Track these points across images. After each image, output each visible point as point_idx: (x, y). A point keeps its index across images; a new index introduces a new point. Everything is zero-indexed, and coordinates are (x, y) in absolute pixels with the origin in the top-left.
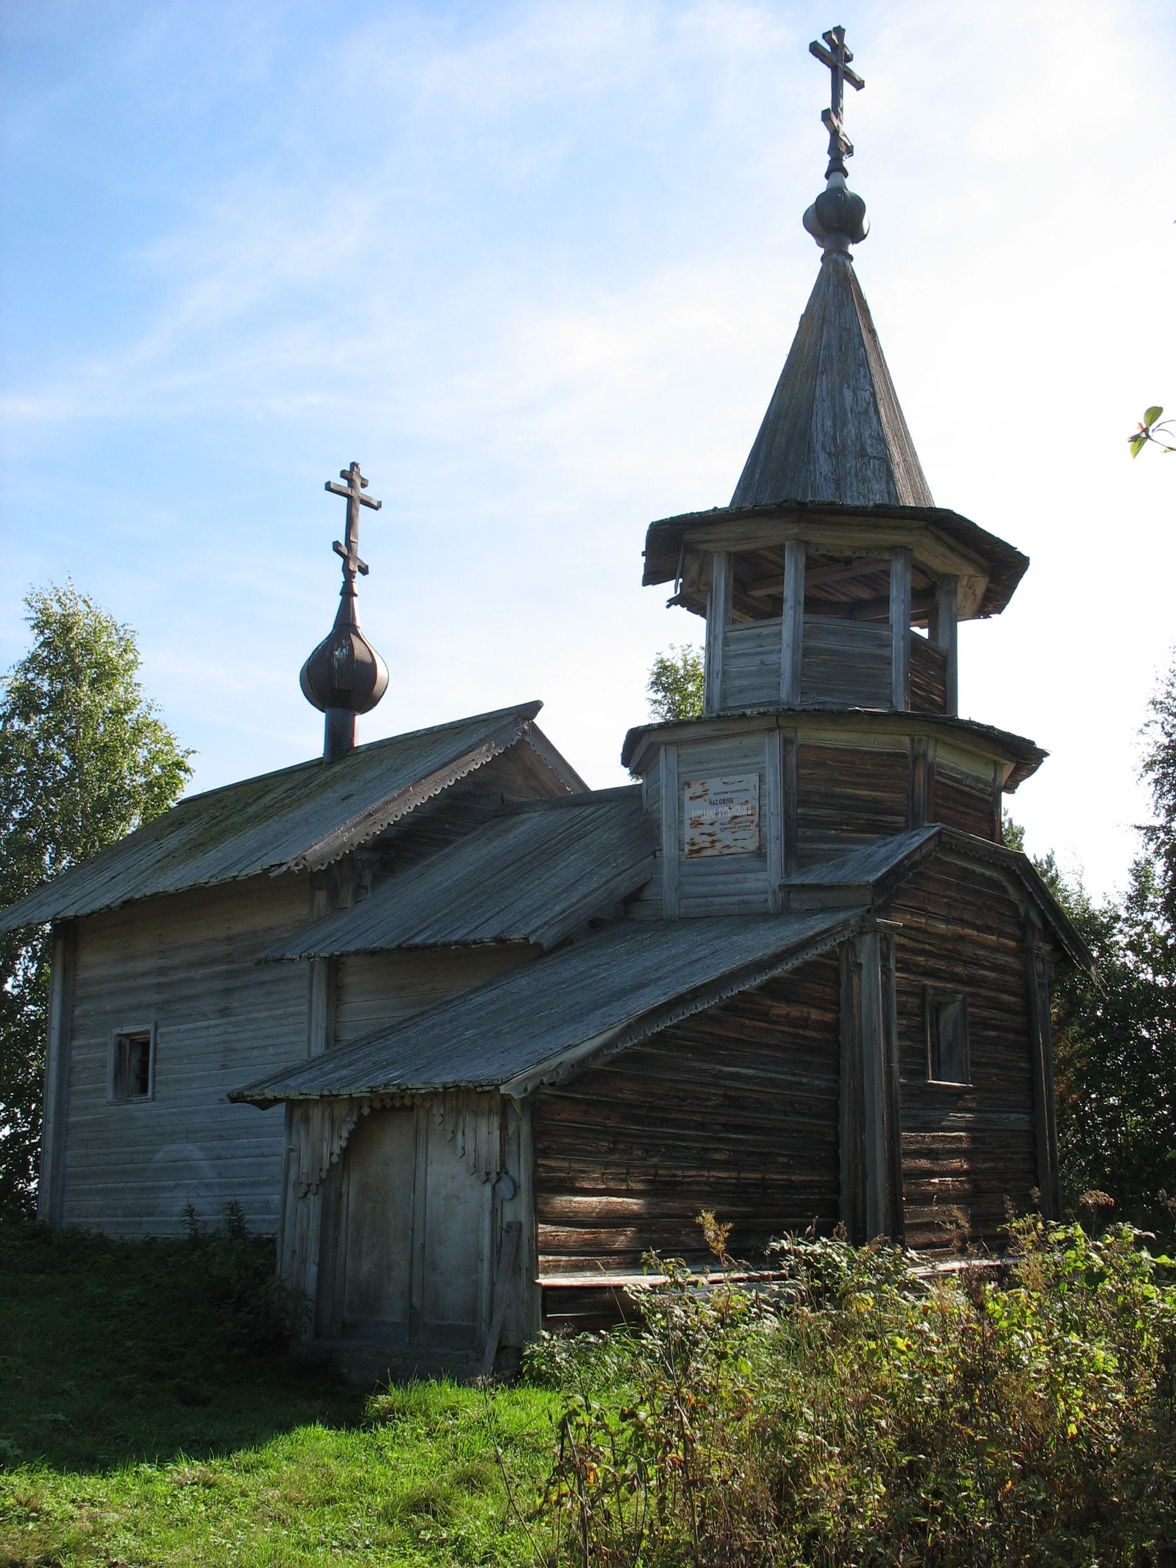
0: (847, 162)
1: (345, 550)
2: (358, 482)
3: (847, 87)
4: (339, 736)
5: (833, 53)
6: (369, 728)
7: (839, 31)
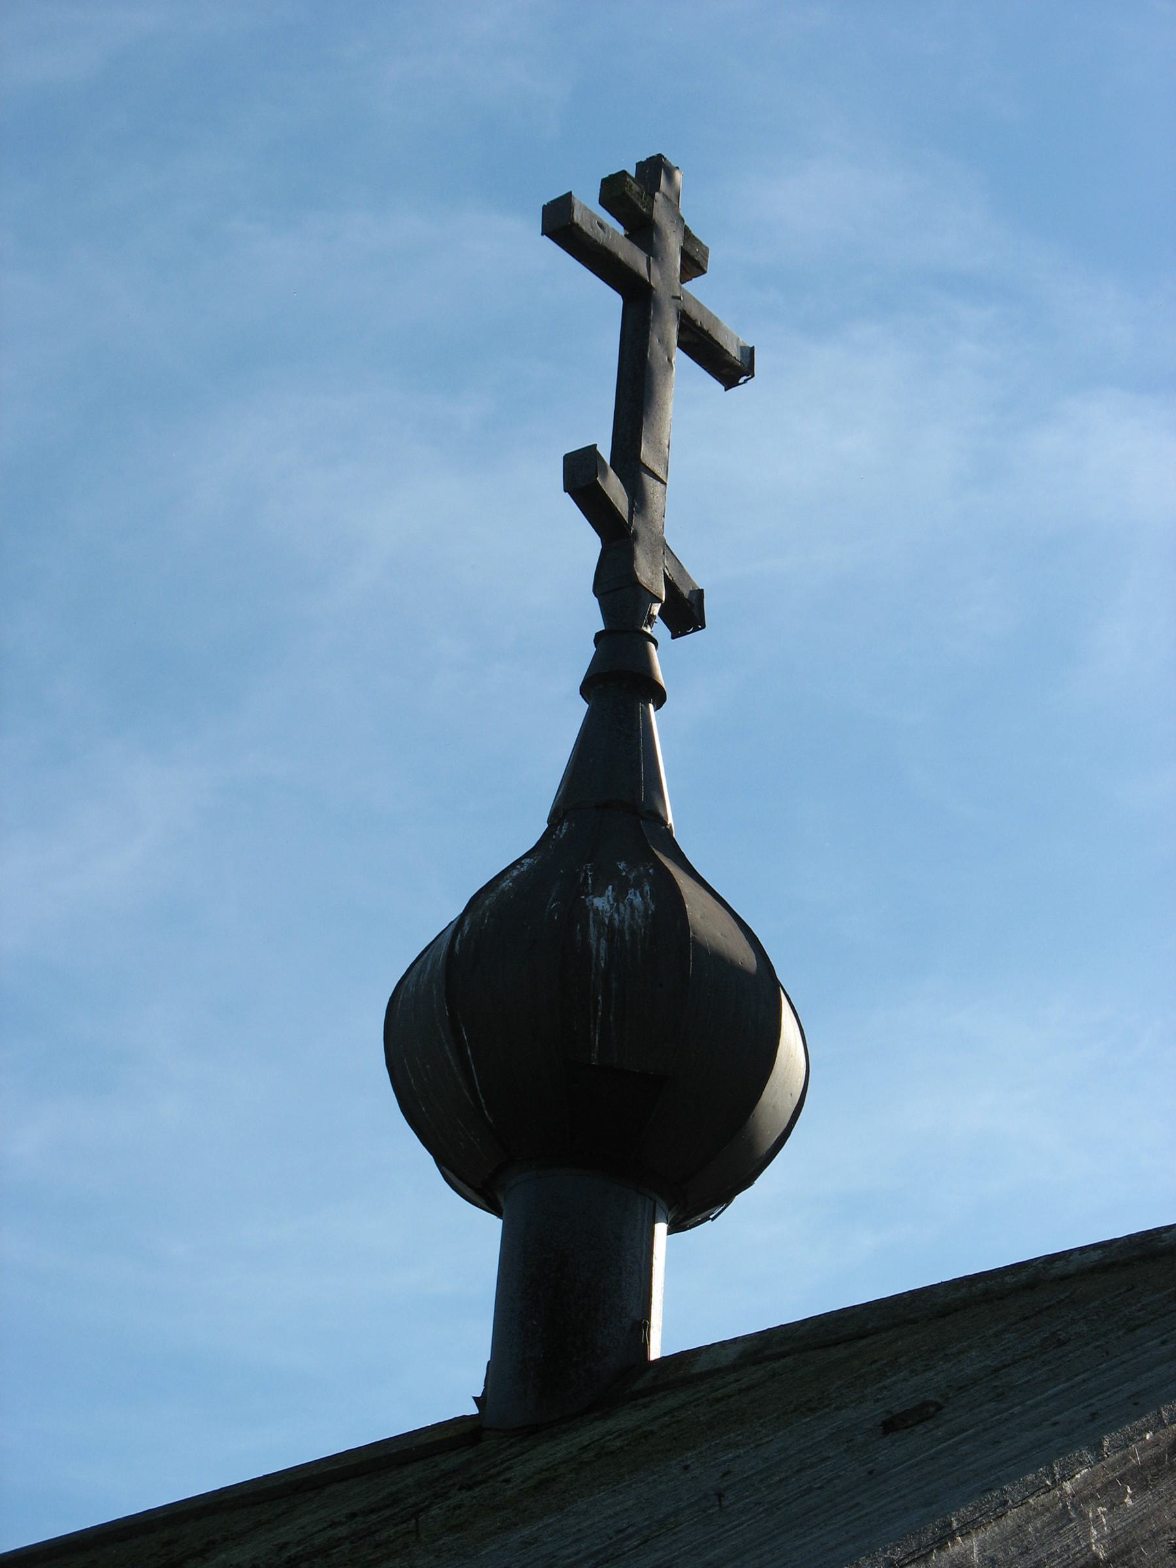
0: (666, 656)
1: (610, 488)
2: (674, 244)
3: (683, 382)
4: (565, 1312)
5: (626, 234)
6: (701, 1288)
7: (655, 169)
